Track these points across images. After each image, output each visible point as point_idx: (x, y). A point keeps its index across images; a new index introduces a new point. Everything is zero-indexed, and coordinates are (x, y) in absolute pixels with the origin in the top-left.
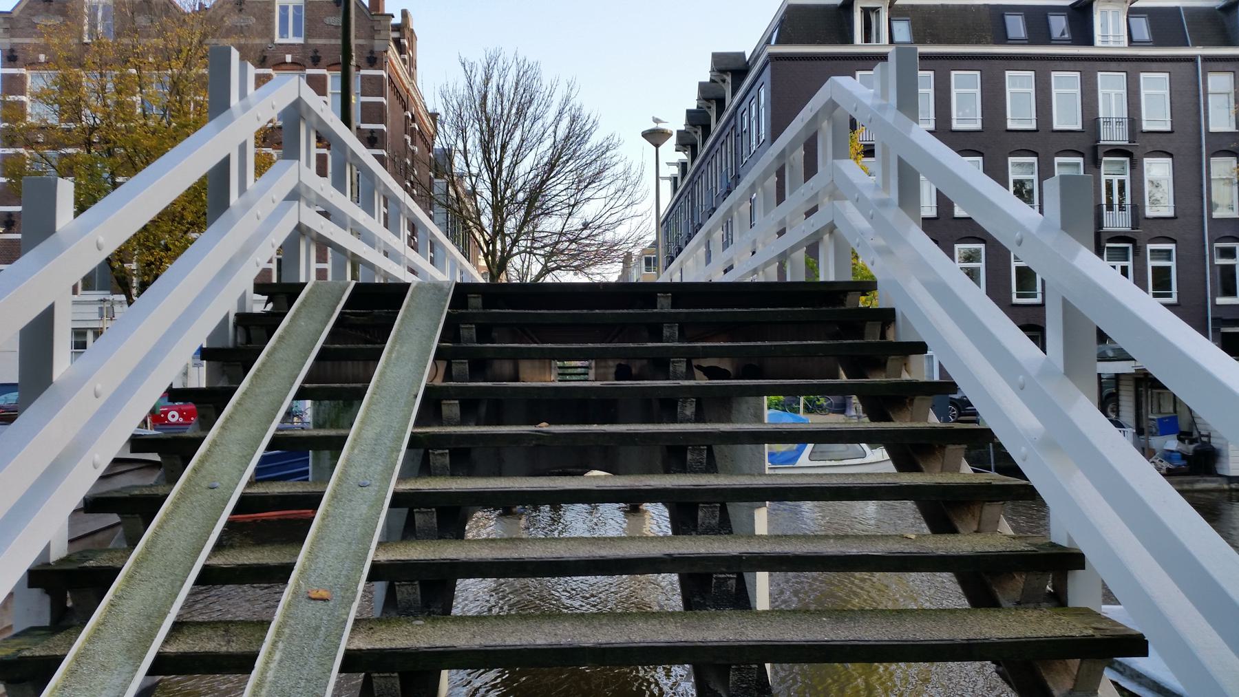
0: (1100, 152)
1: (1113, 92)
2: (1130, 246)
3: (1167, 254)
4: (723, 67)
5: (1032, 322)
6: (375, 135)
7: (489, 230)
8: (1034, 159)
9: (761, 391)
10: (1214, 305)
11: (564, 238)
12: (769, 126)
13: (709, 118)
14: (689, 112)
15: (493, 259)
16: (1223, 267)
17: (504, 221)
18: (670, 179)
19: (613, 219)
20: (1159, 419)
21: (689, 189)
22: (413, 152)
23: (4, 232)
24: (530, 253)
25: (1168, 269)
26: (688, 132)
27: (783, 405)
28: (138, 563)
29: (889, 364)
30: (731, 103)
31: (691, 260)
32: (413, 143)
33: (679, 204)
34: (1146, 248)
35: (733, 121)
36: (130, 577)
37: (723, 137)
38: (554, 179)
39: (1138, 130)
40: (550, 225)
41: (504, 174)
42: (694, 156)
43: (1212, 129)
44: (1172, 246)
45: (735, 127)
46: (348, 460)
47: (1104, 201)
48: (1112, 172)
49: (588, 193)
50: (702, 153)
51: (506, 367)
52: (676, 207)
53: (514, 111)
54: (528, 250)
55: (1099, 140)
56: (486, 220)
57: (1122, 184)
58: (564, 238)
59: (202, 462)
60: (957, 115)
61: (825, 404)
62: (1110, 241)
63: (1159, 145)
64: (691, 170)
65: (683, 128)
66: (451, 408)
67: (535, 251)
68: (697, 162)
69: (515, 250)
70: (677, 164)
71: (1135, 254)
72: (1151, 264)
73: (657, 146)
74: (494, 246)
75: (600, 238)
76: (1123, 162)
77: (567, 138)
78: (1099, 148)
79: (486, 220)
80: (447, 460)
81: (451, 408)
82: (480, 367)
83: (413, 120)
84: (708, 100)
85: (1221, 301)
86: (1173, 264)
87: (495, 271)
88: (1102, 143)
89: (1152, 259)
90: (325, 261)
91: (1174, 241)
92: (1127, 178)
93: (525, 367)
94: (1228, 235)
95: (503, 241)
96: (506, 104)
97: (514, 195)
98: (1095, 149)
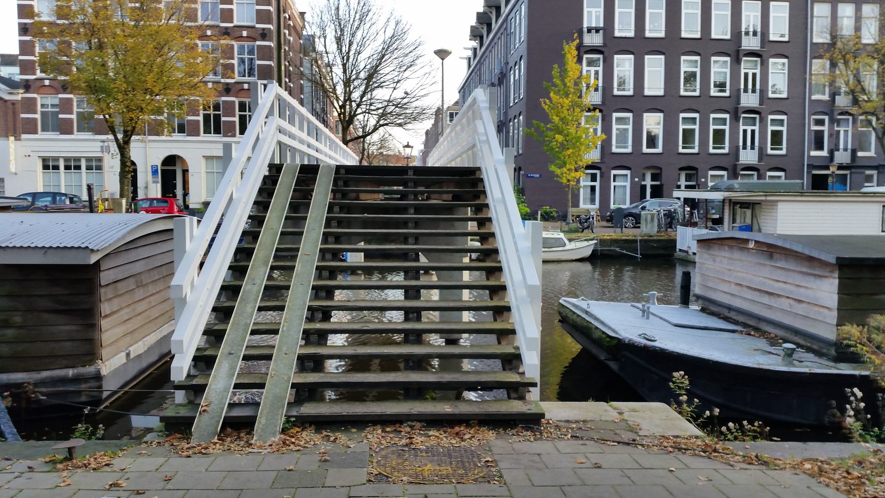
0: (741, 54)
1: (752, 14)
2: (757, 116)
3: (781, 122)
4: (491, 4)
5: (691, 165)
6: (265, 32)
7: (342, 98)
8: (698, 58)
9: (467, 206)
10: (809, 156)
11: (391, 104)
12: (526, 32)
13: (491, 19)
14: (478, 14)
15: (344, 117)
16: (817, 132)
17: (351, 93)
18: (466, 58)
19: (422, 93)
20: (739, 227)
21: (478, 67)
22: (289, 41)
23: (25, 93)
24: (369, 113)
25: (693, 130)
26: (477, 28)
27: (529, 216)
28: (258, 246)
29: (481, 197)
30: (505, 11)
31: (446, 142)
32: (290, 35)
33: (471, 77)
34: (767, 118)
35: (505, 26)
36: (258, 249)
37: (499, 35)
38: (385, 63)
39: (766, 40)
40: (381, 94)
41: (351, 60)
42: (481, 45)
43: (815, 40)
44: (784, 117)
45: (506, 29)
46: (309, 222)
47: (742, 87)
48: (749, 67)
49: (407, 74)
50: (486, 42)
51: (353, 195)
52: (469, 79)
53: (358, 17)
54: (367, 111)
55: (741, 47)
56: (340, 89)
57: (754, 75)
58: (391, 104)
59: (267, 221)
60: (649, 28)
61: (556, 215)
62: (745, 112)
63: (778, 50)
64: (479, 54)
65: (474, 25)
66: (336, 209)
67: (372, 112)
68: (483, 49)
69: (359, 111)
70: (471, 49)
71: (760, 122)
72: (770, 128)
73: (443, 59)
74: (345, 109)
75: (414, 105)
76: (756, 61)
77: (393, 36)
78: (740, 52)
79: (340, 89)
80: (336, 224)
81: (336, 209)
82: (344, 195)
83: (289, 19)
84: (490, 7)
85: (814, 153)
86: (784, 129)
87: (345, 124)
88: (743, 48)
89: (771, 125)
90: (715, 131)
91: (785, 114)
92: (758, 72)
93: (362, 196)
94: (820, 110)
95: (351, 106)
96: (352, 13)
97: (358, 74)
98: (738, 51)
